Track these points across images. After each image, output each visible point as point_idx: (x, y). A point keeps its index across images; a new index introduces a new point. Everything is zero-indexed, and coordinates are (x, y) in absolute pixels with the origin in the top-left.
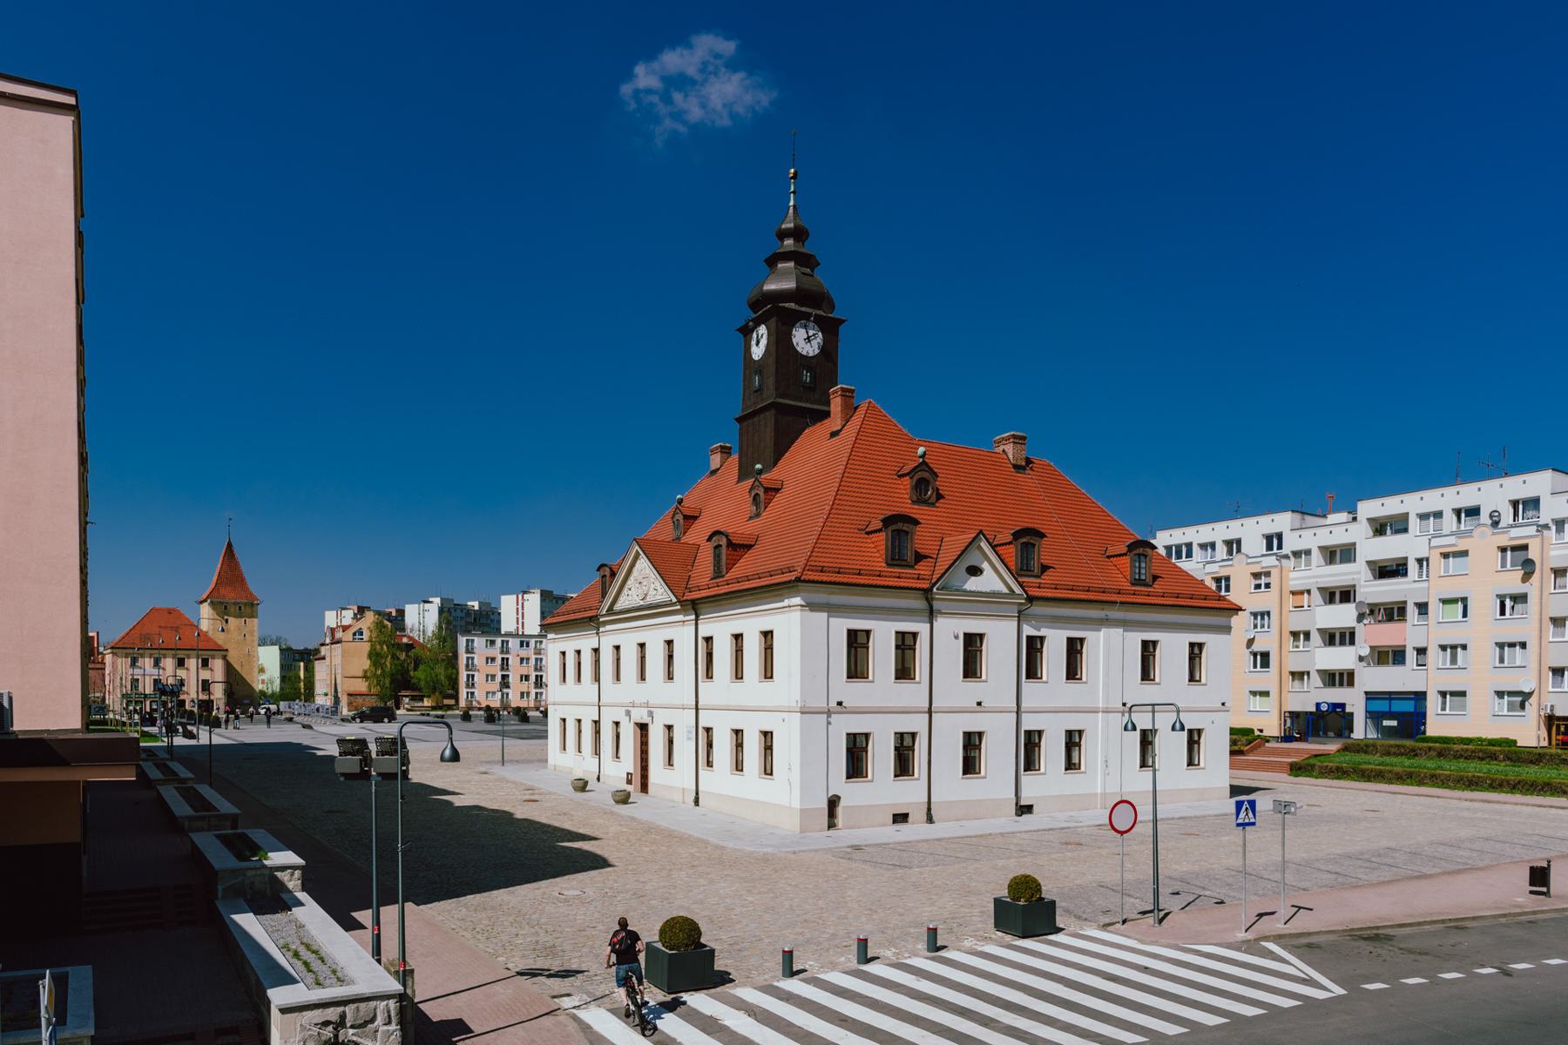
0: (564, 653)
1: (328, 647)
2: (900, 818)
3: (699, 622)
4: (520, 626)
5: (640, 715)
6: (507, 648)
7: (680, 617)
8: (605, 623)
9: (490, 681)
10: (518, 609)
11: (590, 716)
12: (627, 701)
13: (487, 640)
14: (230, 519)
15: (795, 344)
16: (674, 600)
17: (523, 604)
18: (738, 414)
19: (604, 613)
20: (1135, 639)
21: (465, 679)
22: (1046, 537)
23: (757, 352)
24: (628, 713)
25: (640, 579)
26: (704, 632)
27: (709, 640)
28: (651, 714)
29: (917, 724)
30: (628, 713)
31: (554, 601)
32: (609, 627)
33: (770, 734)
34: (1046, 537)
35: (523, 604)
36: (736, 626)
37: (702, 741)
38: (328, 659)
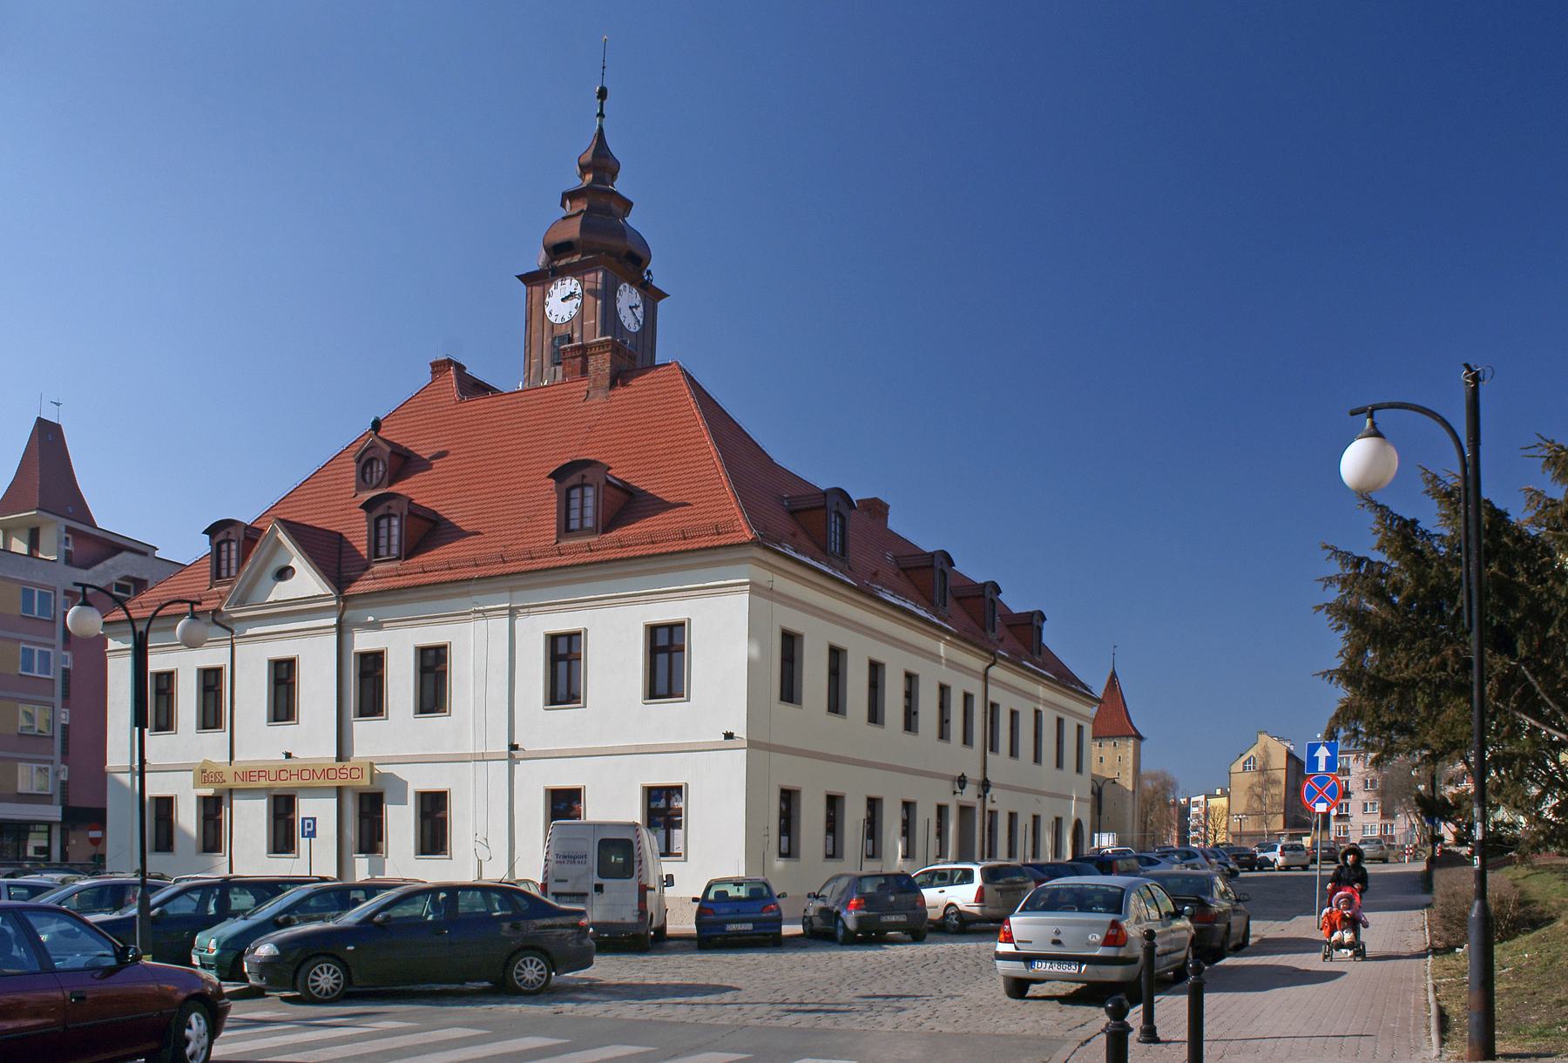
22: (360, 507)
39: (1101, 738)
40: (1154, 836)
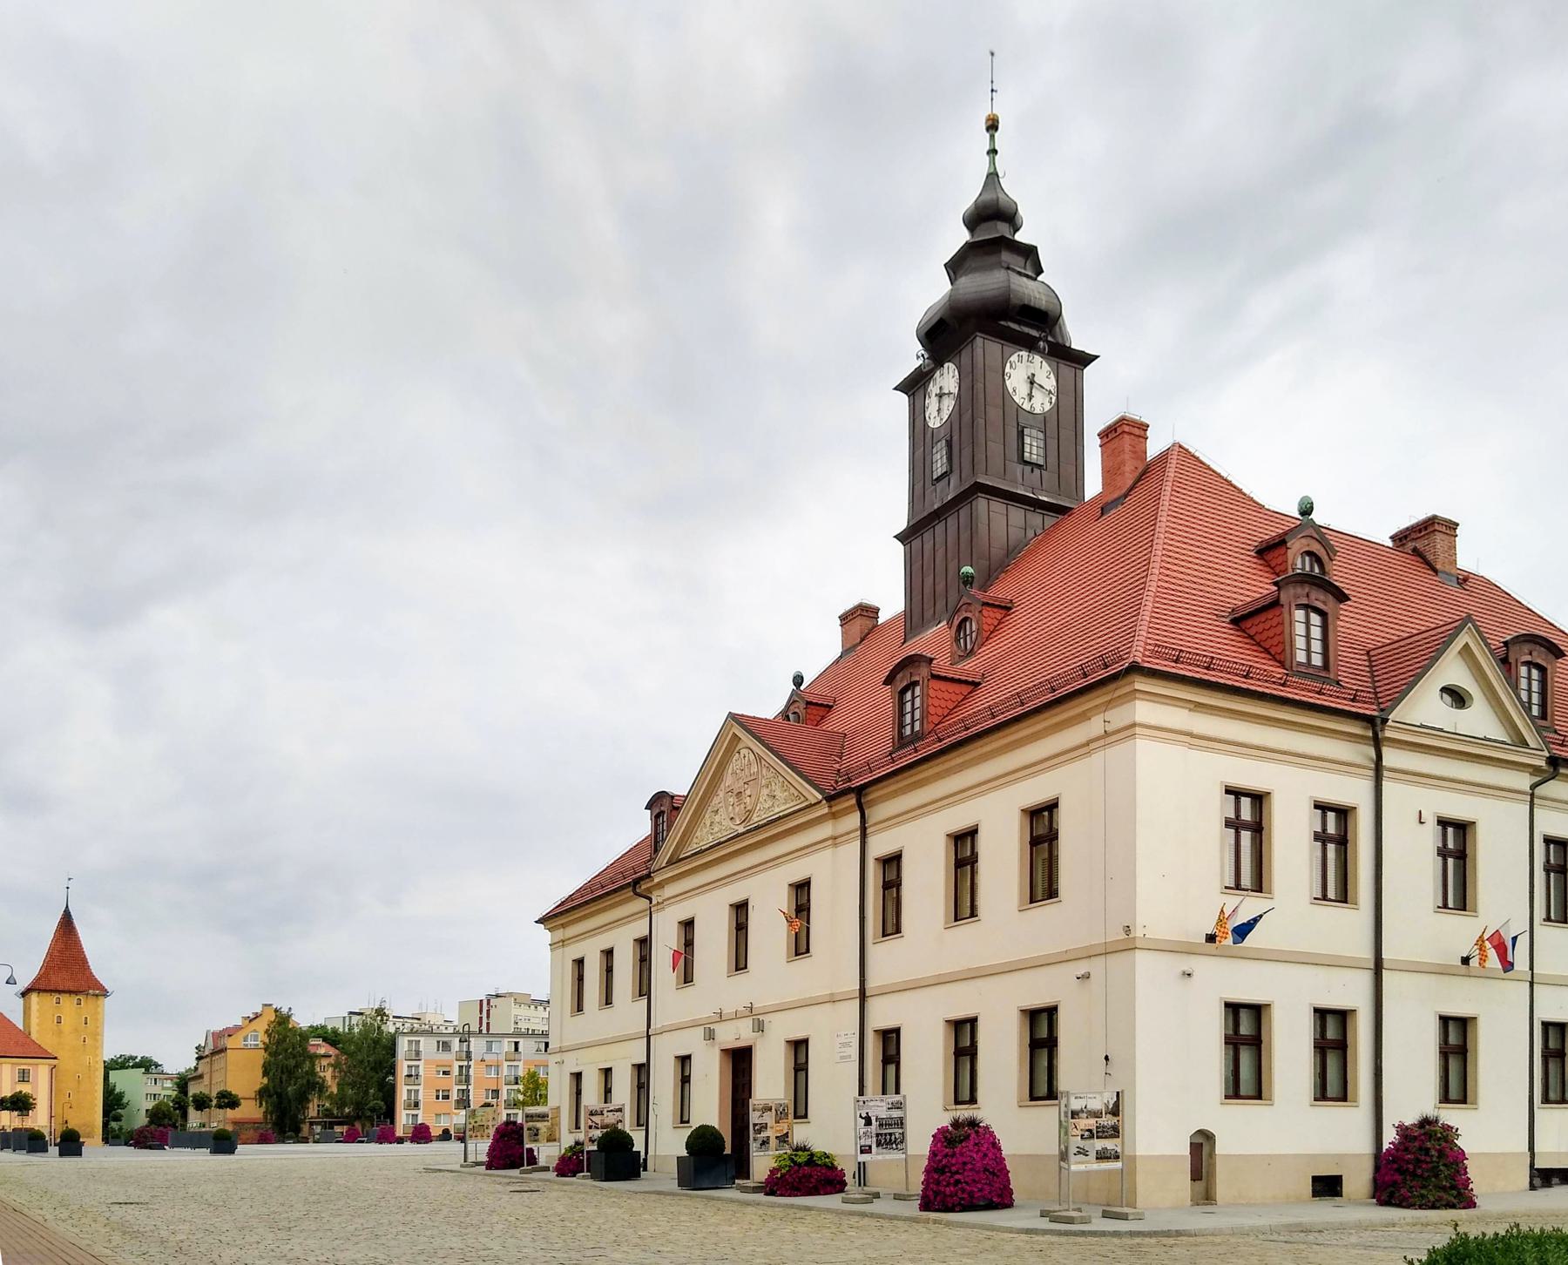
0: (580, 963)
1: (208, 1059)
2: (1327, 1186)
3: (868, 831)
4: (485, 1021)
5: (735, 1034)
6: (468, 1076)
7: (826, 830)
8: (661, 885)
9: (441, 1051)
10: (481, 1018)
11: (622, 1064)
12: (706, 1012)
13: (438, 1042)
14: (70, 879)
15: (1011, 391)
16: (820, 797)
17: (488, 1011)
18: (902, 524)
19: (664, 865)
20: (1071, 1137)
21: (405, 1097)
22: (1350, 599)
23: (938, 414)
24: (710, 1035)
25: (738, 786)
26: (880, 845)
27: (892, 862)
28: (760, 1027)
29: (1351, 992)
30: (710, 1035)
31: (532, 1007)
32: (670, 891)
33: (1044, 1018)
34: (1350, 599)
35: (488, 1011)
36: (604, 941)
37: (874, 1073)
38: (206, 1078)
39: (60, 992)
40: (155, 1095)
